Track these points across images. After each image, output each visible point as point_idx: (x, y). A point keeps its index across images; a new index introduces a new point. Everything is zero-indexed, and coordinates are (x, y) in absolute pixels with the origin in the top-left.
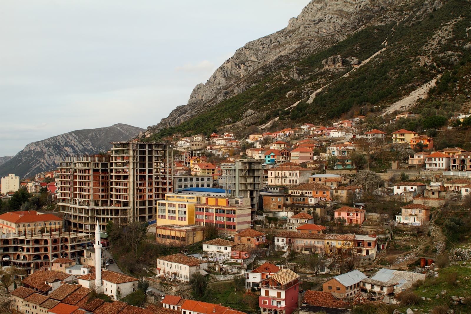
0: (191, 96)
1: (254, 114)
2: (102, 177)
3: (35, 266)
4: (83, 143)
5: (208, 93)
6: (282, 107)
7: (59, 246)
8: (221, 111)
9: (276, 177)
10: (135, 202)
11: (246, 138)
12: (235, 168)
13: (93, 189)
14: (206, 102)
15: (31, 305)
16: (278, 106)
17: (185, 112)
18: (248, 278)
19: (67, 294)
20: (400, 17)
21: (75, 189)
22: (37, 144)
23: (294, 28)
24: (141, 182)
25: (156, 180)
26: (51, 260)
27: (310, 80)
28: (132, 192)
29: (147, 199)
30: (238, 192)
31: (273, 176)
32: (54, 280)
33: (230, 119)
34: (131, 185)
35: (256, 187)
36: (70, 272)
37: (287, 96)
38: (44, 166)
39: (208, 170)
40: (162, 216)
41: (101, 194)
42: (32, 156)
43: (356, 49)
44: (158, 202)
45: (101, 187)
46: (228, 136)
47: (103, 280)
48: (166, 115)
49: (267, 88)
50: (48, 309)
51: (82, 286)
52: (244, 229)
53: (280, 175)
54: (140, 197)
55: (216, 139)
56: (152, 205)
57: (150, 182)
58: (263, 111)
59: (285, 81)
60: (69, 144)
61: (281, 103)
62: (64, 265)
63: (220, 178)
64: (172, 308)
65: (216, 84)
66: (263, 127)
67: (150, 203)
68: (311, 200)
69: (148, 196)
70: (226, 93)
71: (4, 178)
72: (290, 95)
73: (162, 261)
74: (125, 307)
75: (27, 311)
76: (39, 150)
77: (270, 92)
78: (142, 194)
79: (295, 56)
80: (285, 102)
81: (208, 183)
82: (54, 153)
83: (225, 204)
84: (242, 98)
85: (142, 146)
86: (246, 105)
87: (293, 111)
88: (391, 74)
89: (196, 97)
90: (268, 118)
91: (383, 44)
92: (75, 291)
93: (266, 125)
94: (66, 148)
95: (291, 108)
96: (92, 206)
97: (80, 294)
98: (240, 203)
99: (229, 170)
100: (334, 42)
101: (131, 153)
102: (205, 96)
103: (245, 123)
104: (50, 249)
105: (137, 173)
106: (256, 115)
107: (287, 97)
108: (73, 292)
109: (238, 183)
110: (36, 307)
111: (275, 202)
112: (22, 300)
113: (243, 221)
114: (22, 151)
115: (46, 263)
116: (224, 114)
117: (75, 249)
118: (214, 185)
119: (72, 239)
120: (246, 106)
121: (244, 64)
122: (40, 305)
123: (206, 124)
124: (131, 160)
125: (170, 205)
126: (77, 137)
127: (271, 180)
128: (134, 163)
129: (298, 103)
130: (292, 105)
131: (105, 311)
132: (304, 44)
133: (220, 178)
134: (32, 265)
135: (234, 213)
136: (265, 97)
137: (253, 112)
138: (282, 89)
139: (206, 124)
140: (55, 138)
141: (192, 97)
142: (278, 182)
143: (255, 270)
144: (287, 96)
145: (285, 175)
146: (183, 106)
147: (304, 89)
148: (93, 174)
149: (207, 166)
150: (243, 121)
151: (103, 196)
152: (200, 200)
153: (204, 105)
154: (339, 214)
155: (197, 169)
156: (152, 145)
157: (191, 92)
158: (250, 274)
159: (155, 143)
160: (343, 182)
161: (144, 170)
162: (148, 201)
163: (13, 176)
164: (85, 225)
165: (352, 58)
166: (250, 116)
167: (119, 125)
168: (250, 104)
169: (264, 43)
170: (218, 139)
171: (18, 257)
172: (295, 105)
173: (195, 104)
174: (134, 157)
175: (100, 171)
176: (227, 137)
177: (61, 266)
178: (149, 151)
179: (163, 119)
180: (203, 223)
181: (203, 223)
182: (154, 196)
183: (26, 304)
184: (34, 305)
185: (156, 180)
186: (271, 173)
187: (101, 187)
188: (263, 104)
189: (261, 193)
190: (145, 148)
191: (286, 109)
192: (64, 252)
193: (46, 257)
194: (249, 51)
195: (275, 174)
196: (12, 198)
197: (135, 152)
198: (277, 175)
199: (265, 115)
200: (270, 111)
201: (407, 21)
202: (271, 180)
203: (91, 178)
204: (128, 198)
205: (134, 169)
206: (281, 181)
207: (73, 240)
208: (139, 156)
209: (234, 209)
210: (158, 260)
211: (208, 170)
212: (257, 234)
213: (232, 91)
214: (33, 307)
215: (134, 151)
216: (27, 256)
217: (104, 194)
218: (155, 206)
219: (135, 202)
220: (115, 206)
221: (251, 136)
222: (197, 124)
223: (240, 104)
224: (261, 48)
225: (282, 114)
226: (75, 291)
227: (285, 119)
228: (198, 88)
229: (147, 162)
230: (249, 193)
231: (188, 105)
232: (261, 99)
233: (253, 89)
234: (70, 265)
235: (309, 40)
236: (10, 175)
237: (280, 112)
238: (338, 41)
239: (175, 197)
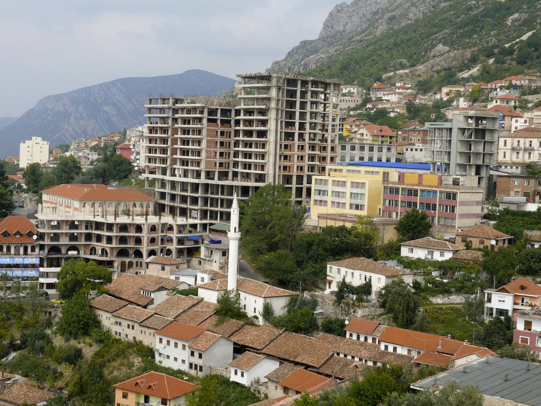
0: (325, 24)
1: (448, 52)
2: (221, 132)
3: (120, 267)
4: (134, 100)
5: (356, 19)
6: (500, 41)
7: (158, 237)
8: (387, 47)
9: (513, 149)
10: (277, 176)
11: (435, 94)
12: (452, 125)
13: (207, 152)
14: (351, 35)
15: (125, 323)
16: (492, 40)
17: (316, 51)
18: (489, 301)
19: (181, 311)
21: (174, 151)
22: (57, 98)
24: (287, 143)
25: (311, 142)
26: (146, 259)
28: (272, 159)
29: (295, 173)
30: (454, 166)
31: (509, 146)
32: (156, 288)
33: (404, 61)
34: (270, 148)
35: (487, 162)
36: (177, 278)
37: (509, 23)
38: (68, 136)
39: (383, 136)
40: (321, 201)
41: (218, 160)
42: (49, 118)
44: (314, 178)
45: (219, 150)
46: (403, 88)
47: (240, 292)
48: (281, 57)
49: (470, 8)
50: (154, 331)
51: (204, 300)
52: (470, 227)
53: (522, 145)
54: (285, 168)
55: (382, 93)
56: (302, 184)
57: (301, 143)
58: (464, 48)
60: (110, 100)
61: (498, 35)
62: (167, 268)
63: (409, 150)
65: (370, 4)
66: (465, 74)
67: (300, 179)
69: (298, 167)
70: (391, 19)
71: (24, 142)
73: (335, 268)
74: (281, 334)
75: (116, 332)
76: (61, 109)
77: (476, 16)
78: (287, 164)
80: (504, 33)
81: (389, 156)
82: (85, 115)
83: (436, 183)
84: (426, 26)
85: (292, 82)
86: (433, 37)
87: (520, 49)
89: (334, 26)
90: (474, 61)
92: (193, 306)
93: (470, 72)
94: (106, 108)
96: (203, 180)
97: (202, 312)
98: (461, 184)
99: (439, 129)
101: (273, 93)
102: (350, 24)
103: (433, 67)
104: (145, 241)
105: (282, 128)
106: (451, 54)
107: (510, 24)
108: (190, 308)
109: (455, 150)
111: (518, 186)
112: (109, 315)
113: (468, 212)
114: (32, 110)
115: (137, 262)
116: (394, 51)
117: (182, 244)
118: (398, 160)
119: (179, 226)
120: (433, 40)
122: (141, 324)
123: (360, 67)
124: (273, 105)
125: (337, 183)
126: (125, 90)
127: (505, 153)
128: (277, 110)
130: (519, 38)
131: (248, 338)
133: (409, 150)
134: (116, 264)
135: (454, 198)
136: (467, 25)
137: (447, 48)
138: (497, 10)
139: (360, 67)
140: (88, 90)
141: (326, 25)
142: (517, 158)
143: (504, 288)
144: (509, 23)
145: (531, 145)
146: (311, 42)
148: (208, 126)
149: (381, 131)
150: (429, 64)
151: (221, 165)
152: (388, 177)
153: (349, 40)
155: (363, 134)
156: (308, 81)
157: (324, 16)
158: (493, 296)
159: (312, 78)
161: (293, 124)
162: (297, 176)
163: (39, 139)
164: (191, 210)
166: (442, 55)
167: (189, 72)
168: (440, 35)
170: (385, 93)
171: (93, 251)
172: (525, 37)
173: (331, 37)
174: (278, 100)
175: (219, 122)
176: (400, 91)
177: (163, 269)
178: (301, 92)
179: (277, 63)
180: (397, 213)
181: (397, 213)
182: (306, 169)
183: (117, 323)
184: (131, 324)
185: (311, 142)
186: (505, 141)
187: (219, 150)
188: (463, 36)
189: (492, 172)
190: (296, 86)
191: (507, 46)
192: (165, 247)
193: (138, 254)
195: (513, 144)
196: (58, 168)
197: (281, 92)
198: (515, 145)
199: (469, 56)
200: (477, 49)
202: (505, 153)
203: (204, 132)
204: (266, 168)
205: (277, 121)
206: (523, 156)
207: (181, 228)
208: (285, 99)
209: (454, 191)
210: (328, 266)
211: (383, 136)
212: (496, 234)
213: (404, 16)
215: (279, 88)
216: (108, 250)
217: (223, 160)
218: (308, 185)
219: (277, 176)
220: (241, 181)
221: (445, 90)
222: (345, 67)
223: (423, 36)
225: (500, 53)
226: (193, 306)
227: (505, 63)
228: (339, 11)
229: (298, 110)
230: (474, 170)
231: (319, 39)
232: (460, 28)
233: (443, 11)
234: (178, 268)
236: (34, 138)
237: (496, 51)
239: (344, 171)
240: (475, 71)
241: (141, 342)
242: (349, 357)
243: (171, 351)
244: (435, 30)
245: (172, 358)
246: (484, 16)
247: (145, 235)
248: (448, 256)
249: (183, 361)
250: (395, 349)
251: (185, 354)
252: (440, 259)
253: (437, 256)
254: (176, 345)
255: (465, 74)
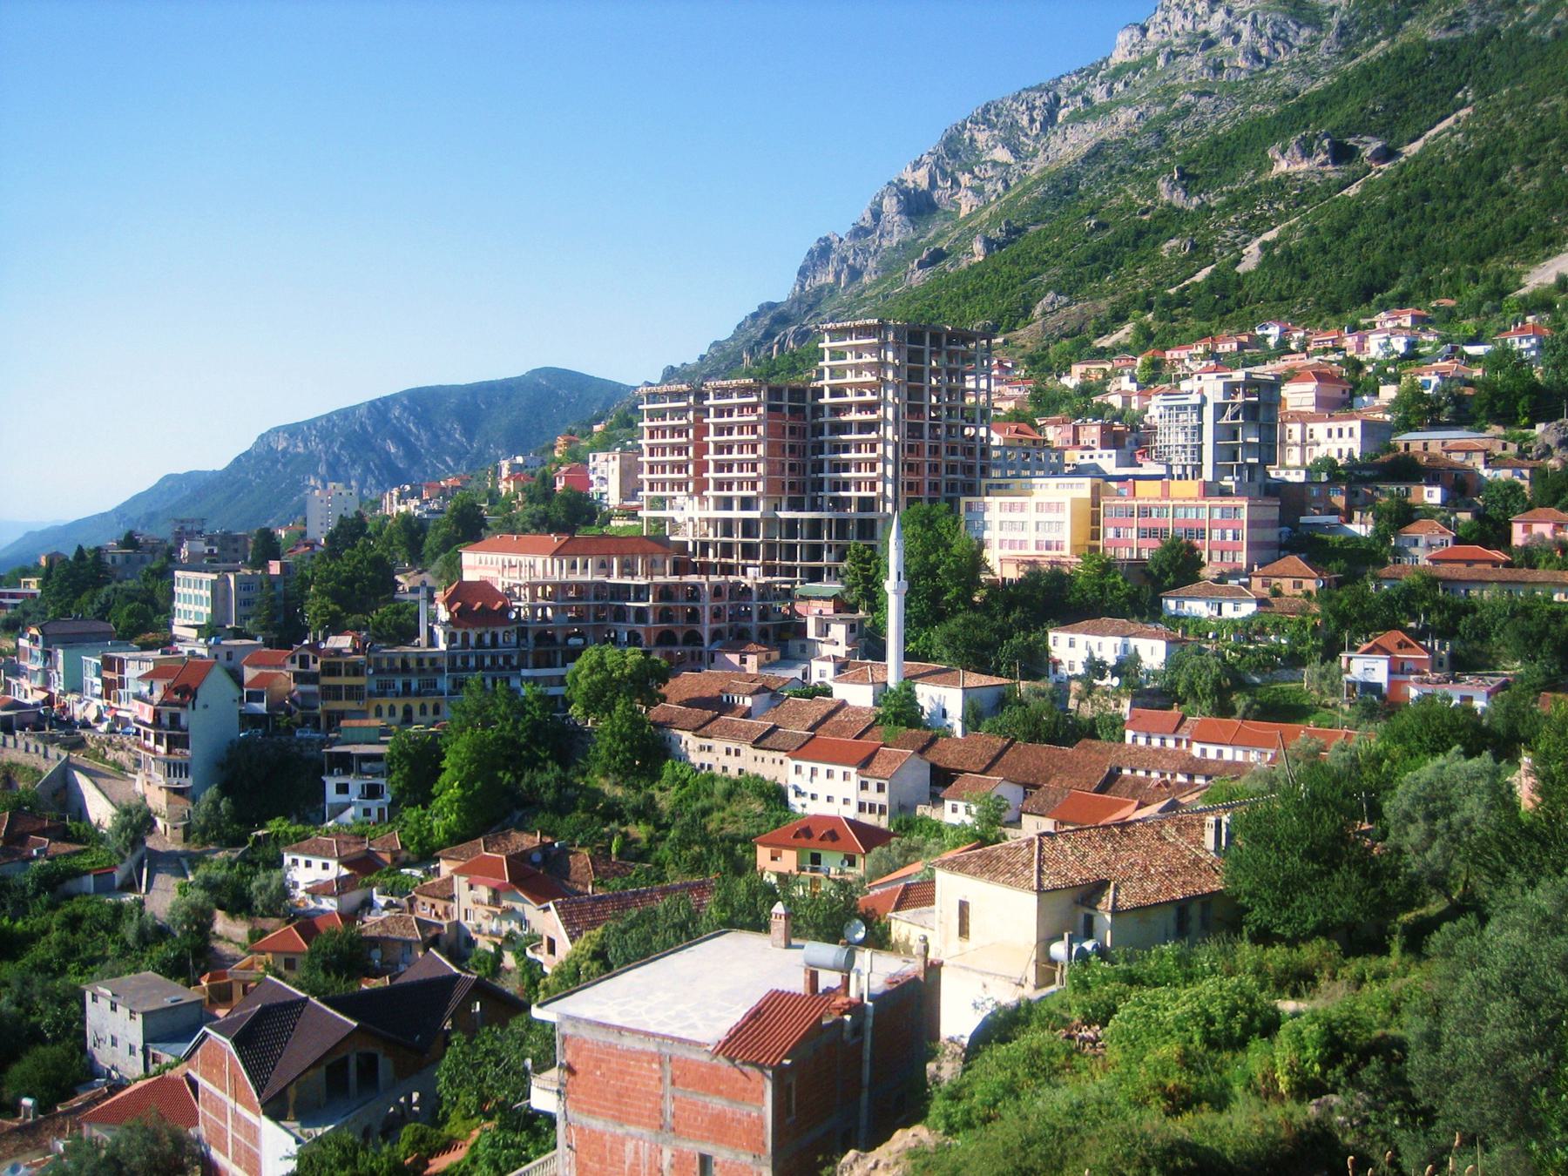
20: (1506, 14)
22: (293, 431)
23: (1135, 57)
27: (1233, 203)
43: (1374, 112)
45: (788, 460)
59: (1144, 213)
64: (1156, 742)
66: (1106, 342)
68: (1430, 494)
72: (1171, 250)
79: (1148, 141)
88: (1514, 180)
90: (1119, 318)
91: (1459, 95)
93: (1115, 338)
95: (1187, 288)
100: (1286, 97)
104: (707, 615)
110: (737, 753)
114: (246, 454)
121: (972, 172)
129: (1207, 270)
132: (1176, 105)
137: (1065, 299)
140: (345, 414)
147: (1217, 231)
154: (1527, 529)
160: (1498, 451)
165: (1365, 139)
169: (1034, 108)
175: (786, 410)
179: (716, 343)
184: (733, 746)
190: (923, 343)
191: (1172, 291)
194: (987, 133)
200: (1117, 297)
201: (1535, 21)
210: (1051, 635)
214: (728, 752)
224: (1025, 121)
235: (1194, 94)
238: (1297, 94)
240: (1124, 333)
241: (757, 776)
242: (1141, 773)
243: (821, 785)
244: (1036, 268)
245: (822, 798)
246: (1118, 244)
247: (707, 605)
248: (1248, 609)
249: (846, 801)
250: (1220, 753)
251: (850, 789)
252: (1237, 615)
253: (1228, 611)
254: (829, 774)
255: (1106, 342)
